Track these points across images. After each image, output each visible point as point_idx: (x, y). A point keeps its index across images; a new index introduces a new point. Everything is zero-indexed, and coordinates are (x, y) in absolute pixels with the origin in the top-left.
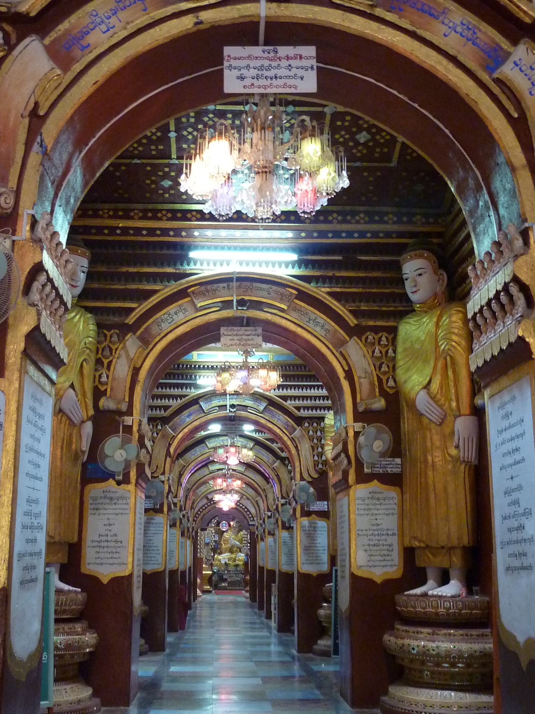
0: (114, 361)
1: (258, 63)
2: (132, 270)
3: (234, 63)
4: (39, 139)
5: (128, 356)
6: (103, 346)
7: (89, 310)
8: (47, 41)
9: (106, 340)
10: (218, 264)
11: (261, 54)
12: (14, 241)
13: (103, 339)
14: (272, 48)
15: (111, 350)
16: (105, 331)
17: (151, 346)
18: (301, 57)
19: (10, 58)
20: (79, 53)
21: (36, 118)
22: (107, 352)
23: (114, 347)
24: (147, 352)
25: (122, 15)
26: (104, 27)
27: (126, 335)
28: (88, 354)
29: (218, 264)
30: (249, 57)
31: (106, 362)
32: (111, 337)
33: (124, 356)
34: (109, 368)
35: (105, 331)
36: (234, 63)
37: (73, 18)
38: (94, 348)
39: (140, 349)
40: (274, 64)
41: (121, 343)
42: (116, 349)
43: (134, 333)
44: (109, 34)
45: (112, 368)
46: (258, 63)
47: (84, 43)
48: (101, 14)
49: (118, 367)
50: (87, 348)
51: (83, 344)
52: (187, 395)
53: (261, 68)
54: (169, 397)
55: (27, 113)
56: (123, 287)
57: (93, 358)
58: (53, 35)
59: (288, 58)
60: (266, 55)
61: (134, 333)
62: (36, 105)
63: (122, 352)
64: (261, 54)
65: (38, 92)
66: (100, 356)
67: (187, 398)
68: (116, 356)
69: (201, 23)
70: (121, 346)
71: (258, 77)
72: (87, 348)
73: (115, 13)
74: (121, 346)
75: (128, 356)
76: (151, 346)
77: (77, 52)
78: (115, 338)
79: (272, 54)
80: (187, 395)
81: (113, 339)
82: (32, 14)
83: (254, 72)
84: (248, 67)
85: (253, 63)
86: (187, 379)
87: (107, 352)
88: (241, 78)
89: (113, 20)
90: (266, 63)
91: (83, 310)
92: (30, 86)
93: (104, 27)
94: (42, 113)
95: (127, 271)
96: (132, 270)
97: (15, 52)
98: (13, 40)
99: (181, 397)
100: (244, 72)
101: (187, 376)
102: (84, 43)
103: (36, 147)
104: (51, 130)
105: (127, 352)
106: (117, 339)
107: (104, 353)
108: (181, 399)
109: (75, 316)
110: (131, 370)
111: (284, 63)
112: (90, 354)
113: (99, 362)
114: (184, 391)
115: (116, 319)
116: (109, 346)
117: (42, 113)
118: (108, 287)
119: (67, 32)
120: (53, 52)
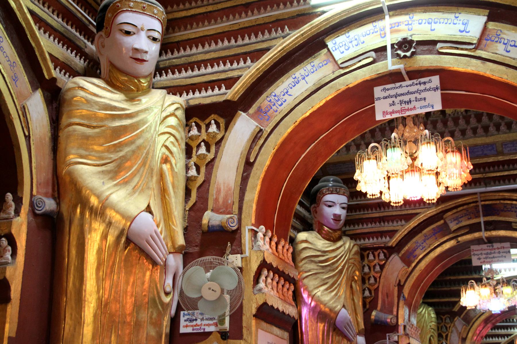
0: (449, 334)
1: (486, 252)
2: (452, 278)
3: (476, 253)
4: (402, 295)
5: (457, 331)
6: (441, 325)
7: (430, 305)
8: (400, 255)
9: (442, 322)
10: (507, 270)
11: (487, 248)
12: (398, 336)
13: (441, 321)
14: (490, 245)
15: (446, 328)
16: (442, 317)
17: (471, 324)
18: (504, 248)
19: (388, 263)
20: (413, 259)
21: (400, 287)
22: (444, 329)
23: (448, 326)
24: (469, 327)
25: (427, 242)
26: (421, 247)
27: (454, 318)
28: (433, 332)
29: (507, 270)
30: (481, 250)
31: (444, 335)
32: (445, 319)
33: (455, 331)
34: (446, 339)
35: (442, 317)
36: (476, 253)
37: (409, 245)
38: (436, 328)
39: (464, 327)
40: (493, 251)
41: (452, 323)
42: (450, 327)
43: (460, 316)
44: (423, 250)
45: (449, 338)
46: (486, 252)
47: (414, 254)
48: (419, 242)
49: (452, 337)
50: (432, 329)
51: (429, 327)
52: (512, 334)
53: (487, 254)
54: (498, 336)
55: (396, 285)
56: (449, 289)
57: (436, 334)
58: (403, 252)
59: (498, 248)
60: (489, 248)
61: (460, 316)
62: (400, 281)
63: (453, 329)
64: (487, 248)
65: (399, 276)
66: (440, 331)
67: (512, 336)
68: (450, 331)
69: (459, 242)
70: (452, 325)
71: (486, 258)
72: (432, 329)
73: (425, 241)
74: (452, 325)
75: (457, 331)
76: (471, 324)
77: (412, 259)
78: (448, 320)
79: (491, 247)
80: (512, 334)
81: (447, 321)
82: (394, 246)
83: (484, 256)
84: (481, 254)
85: (484, 252)
86: (510, 322)
87: (444, 329)
88: (479, 259)
89: (424, 244)
90: (489, 251)
91: (426, 306)
92: (396, 274)
93: (421, 247)
94: (402, 284)
95: (450, 279)
96: (452, 278)
97: (389, 261)
98: (388, 256)
99: (508, 335)
100: (480, 256)
101: (510, 320)
102: (414, 254)
103: (401, 298)
104: (406, 291)
105: (456, 328)
106: (449, 321)
107: (443, 330)
108: (508, 337)
109: (422, 311)
110: (460, 339)
111: (497, 251)
112: (434, 332)
113: (440, 335)
114: (509, 331)
115: (448, 309)
116: (445, 325)
117: (402, 284)
118: (439, 289)
119: (407, 251)
120: (403, 259)
